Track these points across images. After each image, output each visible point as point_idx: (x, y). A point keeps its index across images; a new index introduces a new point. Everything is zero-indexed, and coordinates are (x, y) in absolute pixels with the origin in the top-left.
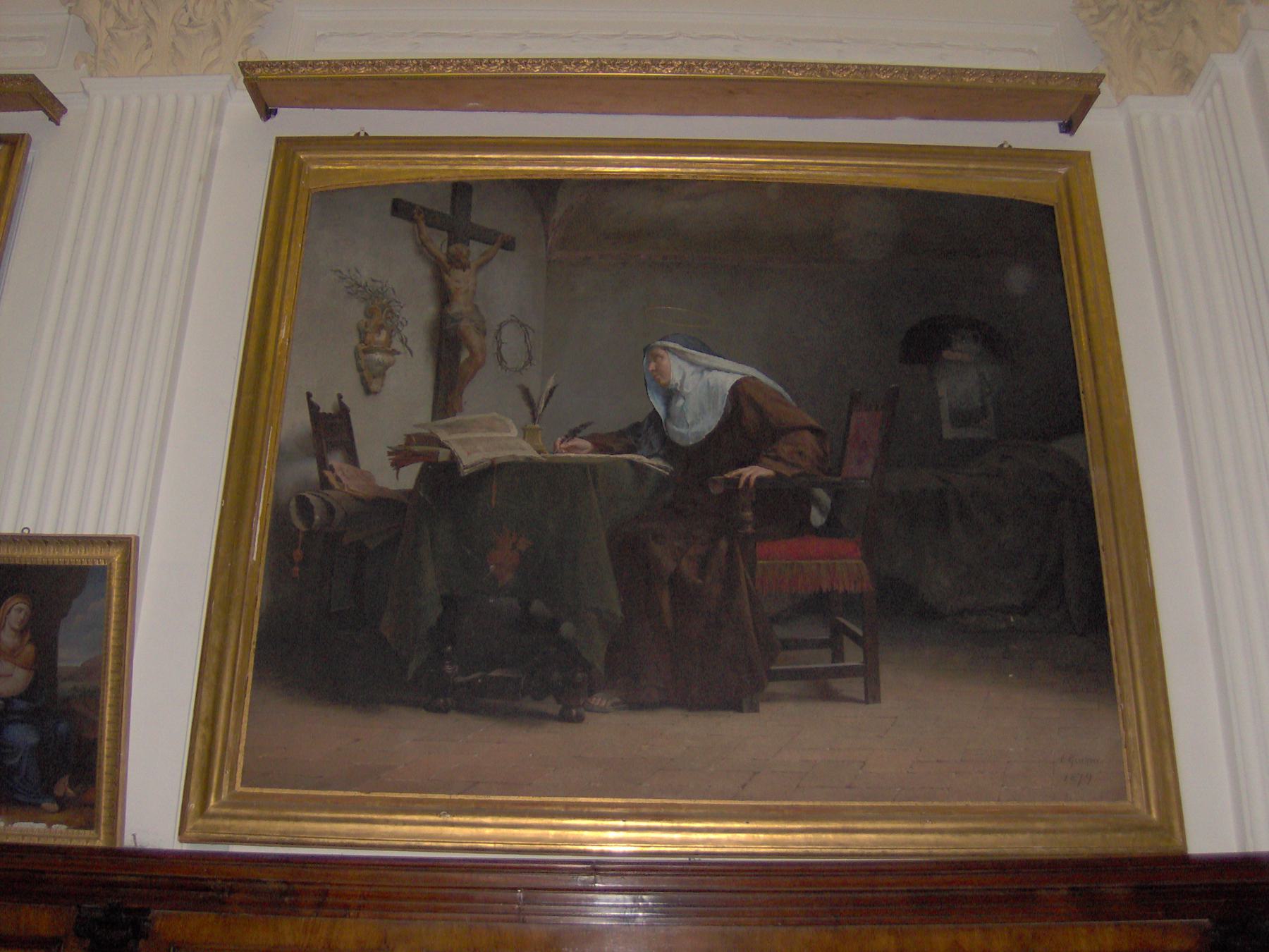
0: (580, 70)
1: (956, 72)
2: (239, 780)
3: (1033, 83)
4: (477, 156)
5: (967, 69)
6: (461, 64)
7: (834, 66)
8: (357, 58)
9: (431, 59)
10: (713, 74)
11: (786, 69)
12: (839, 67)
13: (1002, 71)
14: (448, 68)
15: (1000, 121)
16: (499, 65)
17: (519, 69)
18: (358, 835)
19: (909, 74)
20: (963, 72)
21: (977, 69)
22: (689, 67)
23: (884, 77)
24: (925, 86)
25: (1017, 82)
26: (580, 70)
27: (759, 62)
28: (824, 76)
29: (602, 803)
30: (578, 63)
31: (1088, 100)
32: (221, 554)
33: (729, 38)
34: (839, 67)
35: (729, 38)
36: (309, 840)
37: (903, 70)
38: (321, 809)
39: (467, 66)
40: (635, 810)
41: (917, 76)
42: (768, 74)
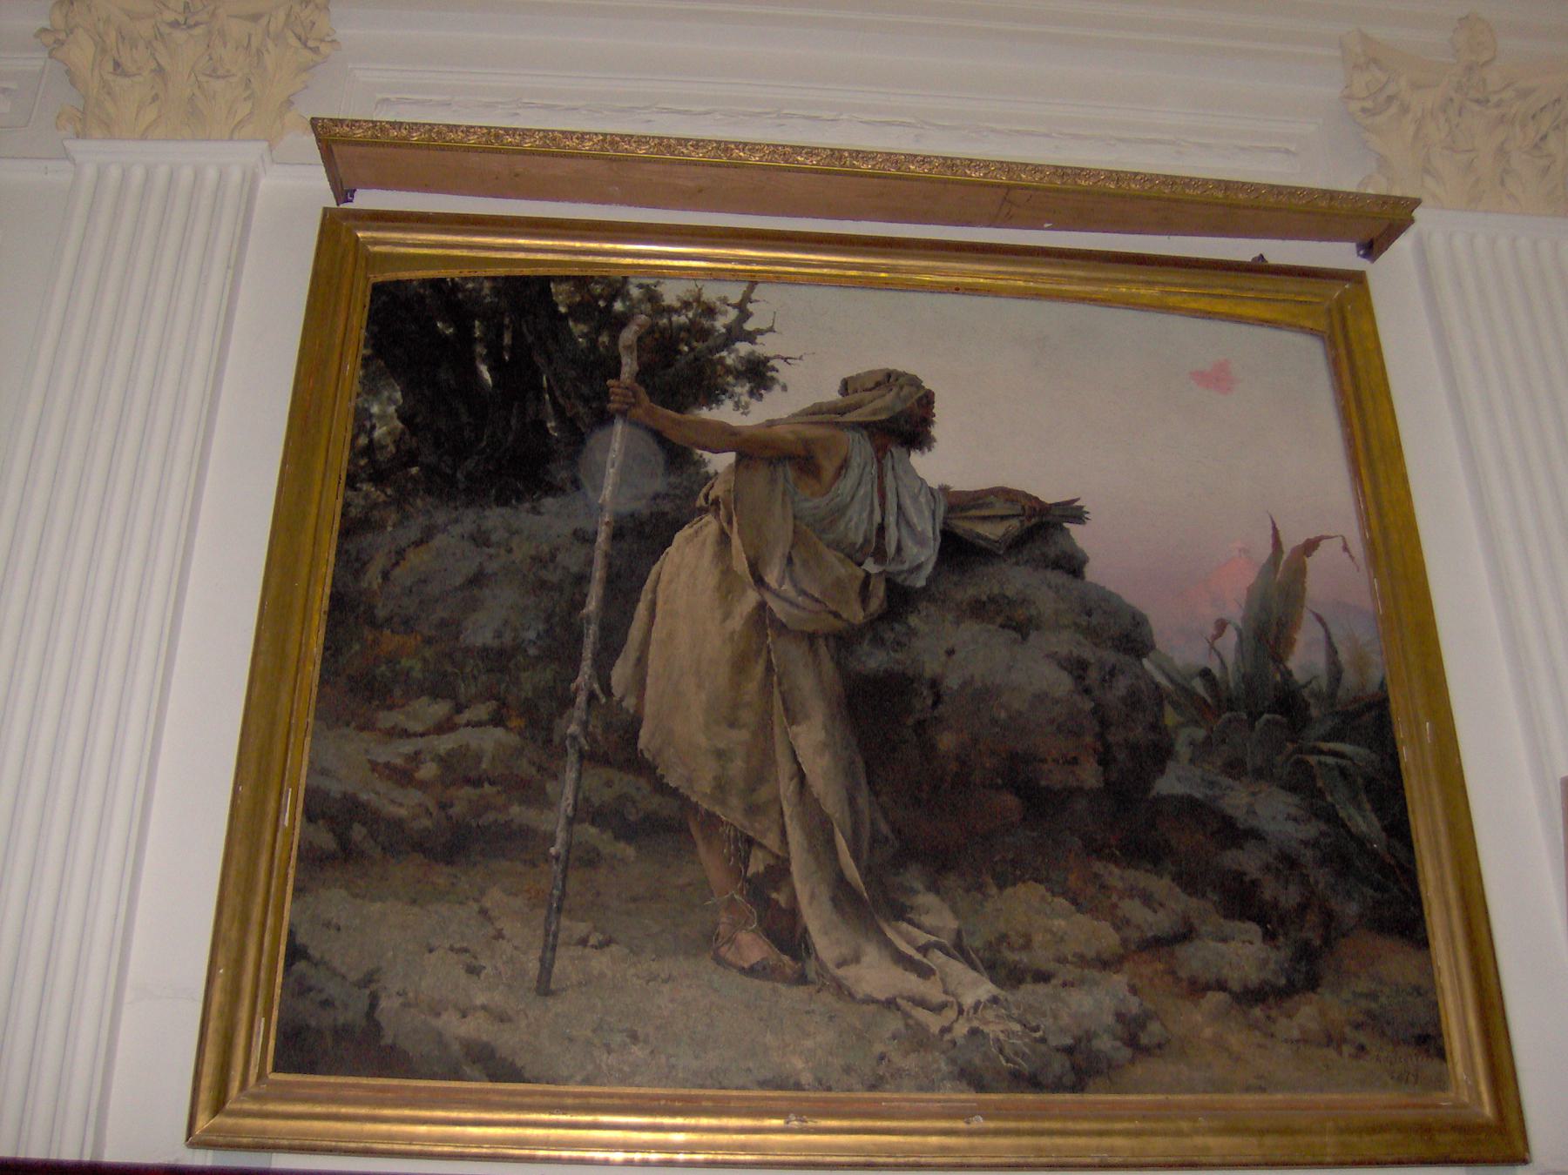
0: (755, 157)
1: (1178, 181)
2: (269, 1067)
3: (1112, 186)
4: (982, 280)
5: (1082, 169)
6: (430, 131)
7: (912, 157)
8: (410, 121)
9: (622, 135)
10: (982, 177)
11: (737, 151)
12: (1030, 168)
13: (1287, 187)
14: (415, 134)
15: (799, 217)
16: (653, 144)
17: (620, 148)
18: (338, 1136)
19: (1008, 172)
20: (1079, 172)
21: (1204, 179)
22: (612, 143)
23: (976, 175)
24: (918, 179)
25: (1252, 197)
26: (698, 154)
27: (818, 148)
28: (899, 169)
29: (515, 1090)
30: (811, 152)
31: (1395, 229)
32: (1457, 759)
33: (909, 125)
34: (1246, 187)
35: (909, 125)
36: (375, 1146)
37: (1003, 165)
38: (383, 1104)
39: (612, 143)
40: (555, 1101)
41: (1019, 175)
42: (940, 173)
